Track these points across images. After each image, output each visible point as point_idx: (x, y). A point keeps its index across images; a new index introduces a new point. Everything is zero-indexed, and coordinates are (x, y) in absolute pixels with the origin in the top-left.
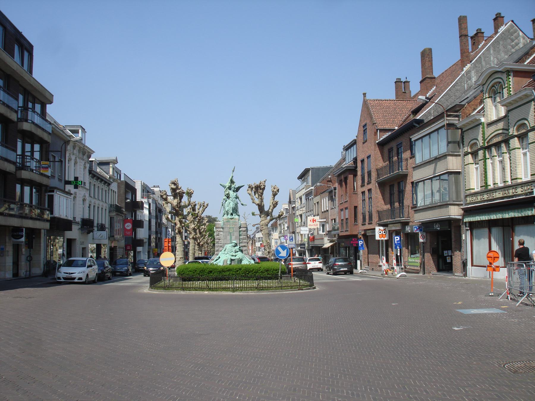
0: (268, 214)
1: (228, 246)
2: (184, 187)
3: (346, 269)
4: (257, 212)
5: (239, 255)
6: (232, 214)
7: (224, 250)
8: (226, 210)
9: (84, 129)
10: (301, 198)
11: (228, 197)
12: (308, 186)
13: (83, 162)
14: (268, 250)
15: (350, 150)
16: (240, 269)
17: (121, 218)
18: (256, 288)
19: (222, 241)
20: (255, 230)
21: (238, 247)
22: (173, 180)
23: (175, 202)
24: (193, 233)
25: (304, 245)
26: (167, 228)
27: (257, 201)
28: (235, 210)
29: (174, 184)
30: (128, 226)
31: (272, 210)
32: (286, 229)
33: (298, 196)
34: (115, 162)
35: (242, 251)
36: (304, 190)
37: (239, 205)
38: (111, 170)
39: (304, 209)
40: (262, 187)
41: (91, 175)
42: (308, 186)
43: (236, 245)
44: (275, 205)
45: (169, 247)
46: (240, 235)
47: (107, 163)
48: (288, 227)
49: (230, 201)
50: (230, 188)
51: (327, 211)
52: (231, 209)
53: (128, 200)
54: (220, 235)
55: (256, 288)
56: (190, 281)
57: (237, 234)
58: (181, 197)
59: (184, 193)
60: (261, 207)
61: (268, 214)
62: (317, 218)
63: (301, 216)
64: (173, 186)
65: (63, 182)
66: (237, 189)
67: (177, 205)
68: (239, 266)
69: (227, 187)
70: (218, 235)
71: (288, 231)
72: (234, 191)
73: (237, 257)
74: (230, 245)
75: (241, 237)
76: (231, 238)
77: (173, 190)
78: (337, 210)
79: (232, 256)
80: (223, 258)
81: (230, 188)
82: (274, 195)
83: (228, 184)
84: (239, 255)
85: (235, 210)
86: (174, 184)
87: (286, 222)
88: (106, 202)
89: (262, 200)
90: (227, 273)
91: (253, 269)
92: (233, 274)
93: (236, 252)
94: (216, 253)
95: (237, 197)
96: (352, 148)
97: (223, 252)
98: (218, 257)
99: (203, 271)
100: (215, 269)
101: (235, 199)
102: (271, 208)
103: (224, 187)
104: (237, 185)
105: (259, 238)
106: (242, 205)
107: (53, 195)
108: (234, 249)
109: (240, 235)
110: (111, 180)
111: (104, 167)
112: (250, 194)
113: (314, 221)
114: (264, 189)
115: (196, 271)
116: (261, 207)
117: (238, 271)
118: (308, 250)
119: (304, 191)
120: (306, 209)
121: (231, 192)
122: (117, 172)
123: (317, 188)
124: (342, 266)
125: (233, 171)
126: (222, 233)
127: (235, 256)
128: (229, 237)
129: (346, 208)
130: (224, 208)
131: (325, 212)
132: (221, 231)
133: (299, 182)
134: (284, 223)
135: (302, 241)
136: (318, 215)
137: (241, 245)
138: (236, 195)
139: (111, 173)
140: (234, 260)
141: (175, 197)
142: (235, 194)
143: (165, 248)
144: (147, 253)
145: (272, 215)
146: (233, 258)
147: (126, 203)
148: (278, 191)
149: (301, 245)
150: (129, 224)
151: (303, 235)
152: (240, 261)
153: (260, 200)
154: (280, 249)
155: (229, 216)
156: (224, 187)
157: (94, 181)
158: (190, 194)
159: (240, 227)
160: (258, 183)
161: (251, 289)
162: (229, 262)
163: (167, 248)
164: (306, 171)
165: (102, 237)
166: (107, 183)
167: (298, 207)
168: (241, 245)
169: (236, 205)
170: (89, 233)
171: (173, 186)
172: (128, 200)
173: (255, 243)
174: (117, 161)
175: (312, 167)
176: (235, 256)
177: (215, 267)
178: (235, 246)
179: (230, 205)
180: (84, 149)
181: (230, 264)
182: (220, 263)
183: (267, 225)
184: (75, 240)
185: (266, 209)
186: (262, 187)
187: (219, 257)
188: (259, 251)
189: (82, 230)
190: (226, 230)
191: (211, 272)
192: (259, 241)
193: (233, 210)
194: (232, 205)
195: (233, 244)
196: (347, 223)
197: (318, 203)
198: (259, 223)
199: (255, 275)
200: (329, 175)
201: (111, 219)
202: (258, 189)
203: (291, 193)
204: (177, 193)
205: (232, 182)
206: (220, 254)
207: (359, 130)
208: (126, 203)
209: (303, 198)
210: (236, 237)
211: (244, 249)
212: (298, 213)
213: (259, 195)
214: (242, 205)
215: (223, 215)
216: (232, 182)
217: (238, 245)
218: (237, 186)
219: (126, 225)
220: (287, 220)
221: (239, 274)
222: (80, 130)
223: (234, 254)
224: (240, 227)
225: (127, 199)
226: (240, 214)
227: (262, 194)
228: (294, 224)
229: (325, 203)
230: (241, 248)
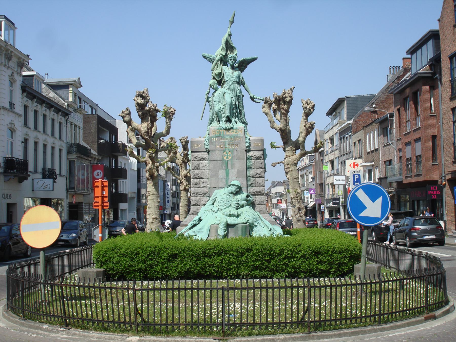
0: (297, 145)
1: (221, 194)
2: (157, 101)
3: (434, 237)
4: (279, 142)
5: (247, 214)
6: (229, 120)
7: (210, 202)
8: (217, 109)
10: (332, 140)
11: (220, 83)
12: (344, 119)
13: (9, 72)
14: (298, 206)
15: (419, 52)
16: (249, 250)
17: (87, 163)
18: (301, 323)
19: (206, 182)
20: (271, 184)
21: (244, 195)
22: (140, 90)
23: (144, 127)
24: (185, 182)
25: (338, 199)
26: (165, 182)
27: (279, 125)
28: (236, 111)
29: (141, 96)
30: (97, 174)
31: (304, 139)
32: (310, 180)
33: (327, 136)
34: (77, 84)
35: (253, 205)
36: (337, 127)
37: (246, 100)
38: (71, 95)
39: (337, 152)
40: (288, 99)
41: (25, 94)
42: (344, 119)
43: (239, 191)
44: (309, 130)
45: (103, 197)
46: (248, 168)
47: (65, 86)
48: (313, 179)
49: (224, 90)
50: (224, 61)
51: (377, 150)
52: (227, 107)
53: (102, 141)
54: (204, 169)
55: (301, 323)
56: (122, 278)
57: (240, 165)
58: (154, 119)
59: (159, 111)
60: (285, 134)
61: (297, 145)
62: (359, 161)
63: (332, 162)
64: (140, 101)
66: (243, 65)
67: (147, 132)
68: (246, 241)
69: (218, 57)
70: (197, 168)
71: (314, 183)
72: (233, 68)
73: (241, 220)
74: (226, 190)
75: (252, 172)
76: (227, 174)
77: (141, 107)
78: (395, 145)
79: (230, 216)
80: (206, 222)
81: (224, 61)
82: (307, 114)
83: (219, 52)
84: (247, 214)
85: (236, 111)
86: (141, 96)
87: (310, 172)
88: (60, 138)
89: (287, 124)
90: (216, 260)
91: (282, 250)
92: (230, 263)
93: (239, 206)
95: (240, 82)
96: (424, 48)
97: (208, 206)
98: (197, 218)
100: (187, 249)
101: (235, 85)
102: (303, 135)
103: (211, 60)
104: (241, 54)
105: (276, 193)
106: (253, 99)
108: (234, 200)
109: (248, 168)
110: (71, 109)
111: (61, 92)
112: (266, 114)
113: (355, 165)
114: (290, 103)
115: (137, 254)
116: (285, 134)
117: (242, 254)
118: (342, 205)
119: (337, 129)
120: (340, 152)
121: (227, 70)
122: (80, 98)
123: (356, 123)
124: (426, 232)
125: (232, 22)
126: (205, 163)
127: (238, 216)
128: (222, 173)
129: (417, 140)
130: (212, 106)
131: (372, 152)
132: (204, 159)
133: (328, 119)
134: (308, 174)
135: (333, 194)
136: (360, 157)
137: (251, 190)
138: (239, 77)
139: (71, 99)
140: (233, 226)
141: (143, 118)
142: (236, 73)
143: (97, 200)
144: (135, 212)
145: (303, 147)
146: (232, 221)
147: (99, 145)
148: (313, 107)
149: (334, 199)
150: (99, 171)
151: (336, 187)
152: (250, 227)
153: (283, 122)
154: (362, 196)
155: (223, 124)
156: (211, 60)
157: (33, 105)
158: (169, 115)
159: (248, 150)
160: (280, 94)
162: (221, 232)
163: (99, 200)
164: (340, 102)
165: (46, 187)
166: (65, 114)
167: (327, 151)
168: (251, 190)
169: (239, 98)
170: (21, 180)
171: (140, 101)
172: (102, 141)
173: (271, 199)
174: (80, 84)
175: (348, 95)
176: (238, 216)
177: (186, 243)
178: (236, 193)
179: (224, 98)
180: (7, 50)
181: (226, 236)
182: (201, 234)
183: (296, 164)
185: (294, 137)
186: (288, 99)
187: (200, 220)
188: (276, 208)
189: (5, 176)
190: (215, 155)
191: (175, 256)
192: (276, 197)
193: (231, 109)
194: (229, 98)
195: (233, 189)
196: (418, 163)
197: (360, 141)
198: (282, 160)
199: (287, 265)
200: (373, 104)
201: (71, 163)
202: (282, 104)
203: (318, 134)
204: (148, 114)
206: (203, 212)
207: (443, 9)
208: (99, 145)
209: (336, 140)
210: (239, 171)
211: (258, 199)
212: (328, 159)
213: (282, 114)
214: (253, 99)
215: (208, 121)
216: (229, 47)
217: (244, 190)
218: (239, 59)
219: (95, 173)
220: (311, 169)
221: (247, 261)
222: (3, 23)
223: (234, 211)
224: (248, 150)
225: (99, 139)
226: (247, 120)
227: (287, 111)
228: (321, 173)
229: (373, 140)
230: (251, 198)
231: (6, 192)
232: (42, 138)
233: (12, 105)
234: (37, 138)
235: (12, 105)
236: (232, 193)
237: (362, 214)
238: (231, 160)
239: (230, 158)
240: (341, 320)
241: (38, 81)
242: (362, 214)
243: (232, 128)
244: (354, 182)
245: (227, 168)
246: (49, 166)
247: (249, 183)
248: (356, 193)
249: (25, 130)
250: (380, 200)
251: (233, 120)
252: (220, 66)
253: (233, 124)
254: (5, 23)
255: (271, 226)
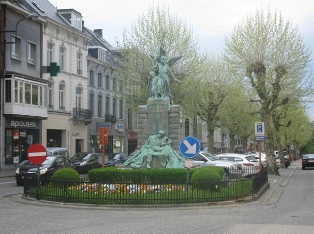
9: (80, 14)
46: (170, 123)
49: (158, 77)
65: (38, 68)
74: (155, 136)
94: (138, 146)
99: (113, 173)
107: (10, 81)
132: (145, 118)
155: (156, 98)
161: (109, 207)
184: (64, 131)
187: (141, 153)
205: (163, 52)
223: (158, 148)
231: (75, 132)
232: (104, 93)
233: (79, 71)
234: (100, 93)
235: (79, 71)
236: (159, 138)
237: (186, 152)
238: (160, 118)
239: (159, 117)
240: (146, 200)
241: (102, 53)
242: (186, 152)
243: (160, 100)
244: (258, 130)
245: (157, 123)
246: (111, 113)
247: (170, 132)
248: (184, 142)
249: (91, 88)
250: (195, 145)
251: (162, 95)
252: (157, 63)
253: (162, 97)
254: (31, 47)
255: (180, 157)
